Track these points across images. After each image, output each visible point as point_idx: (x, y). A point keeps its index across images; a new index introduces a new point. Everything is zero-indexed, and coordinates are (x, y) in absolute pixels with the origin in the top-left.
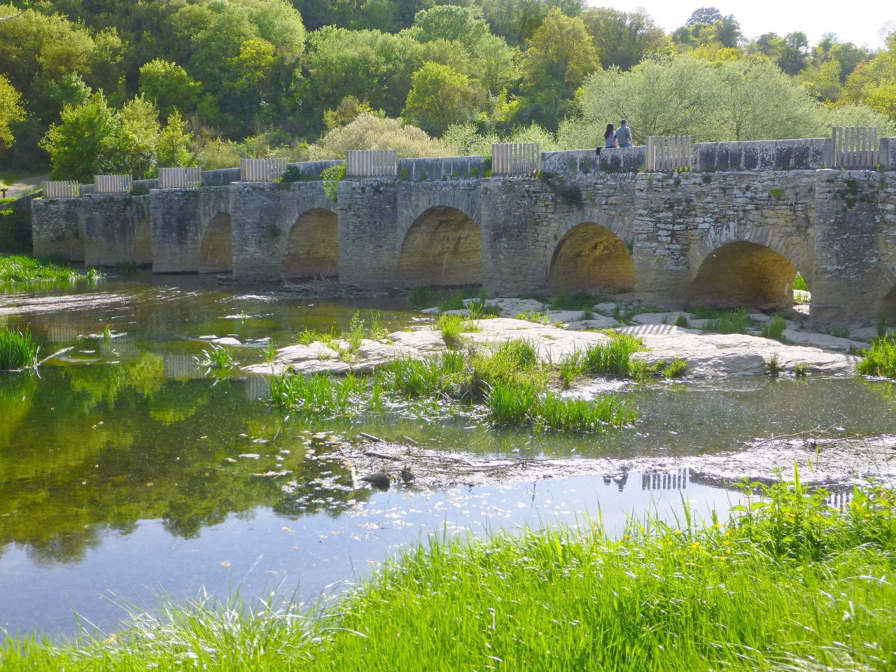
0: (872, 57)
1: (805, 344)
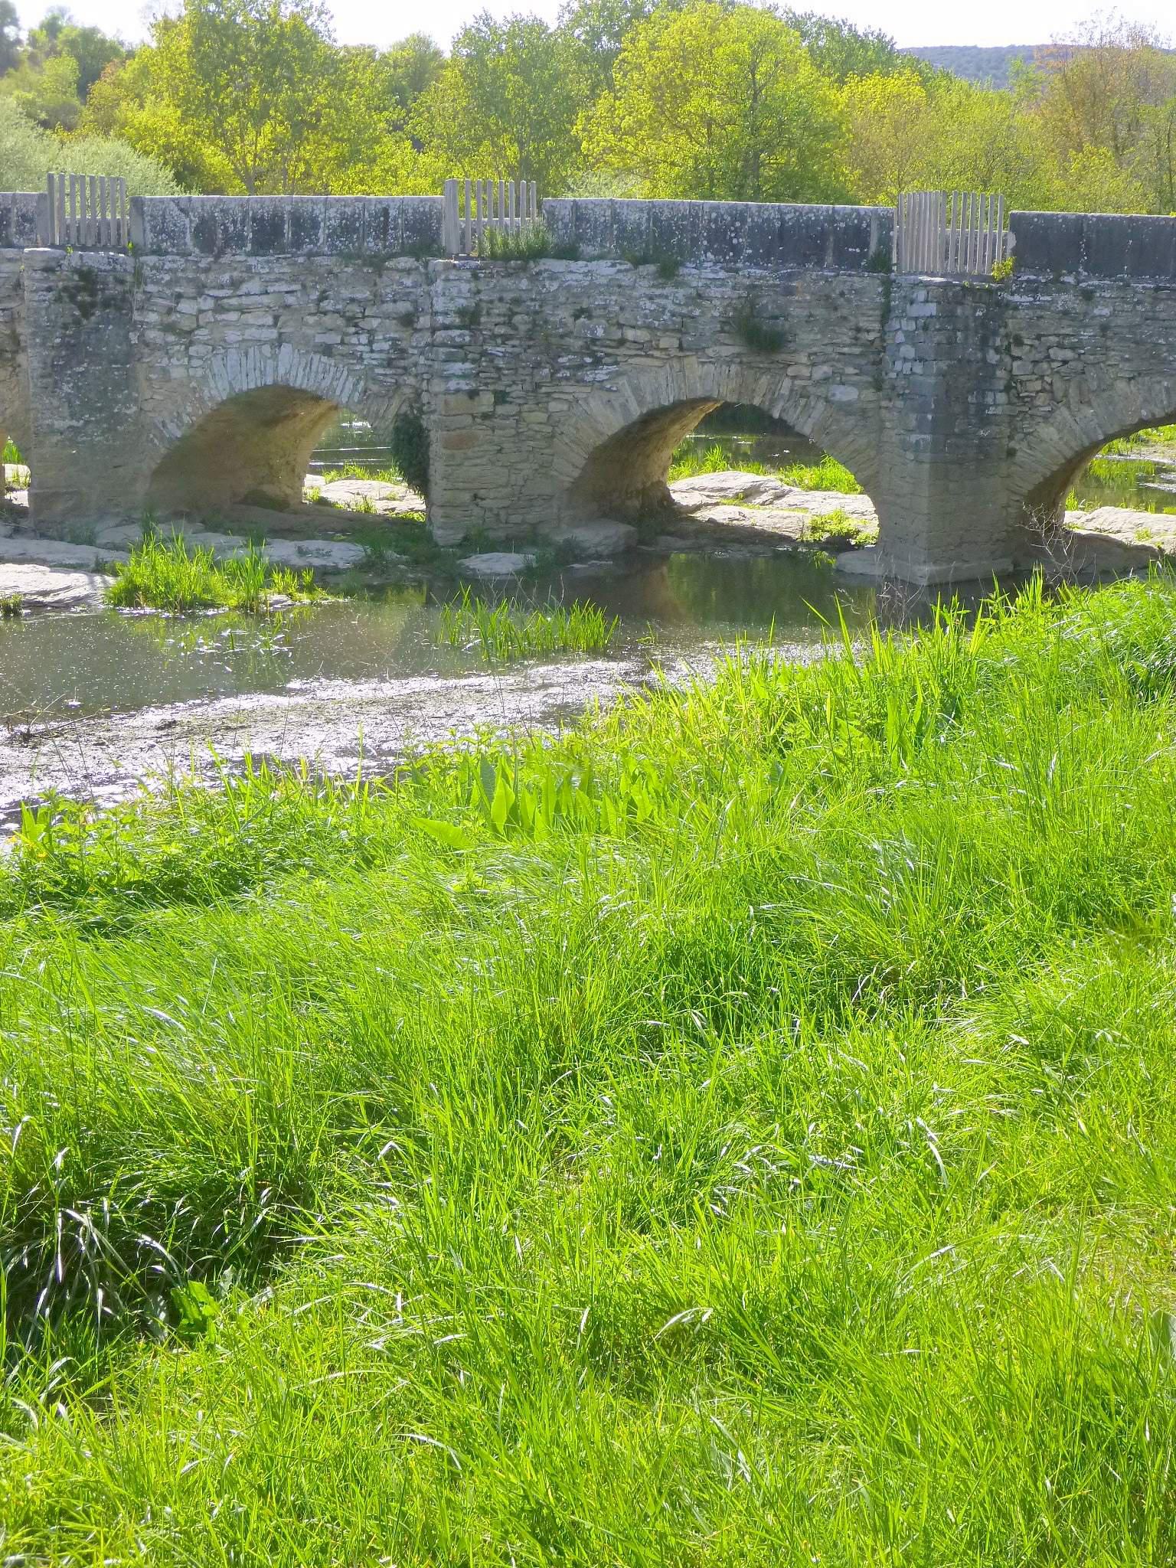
0: (131, 55)
1: (22, 559)
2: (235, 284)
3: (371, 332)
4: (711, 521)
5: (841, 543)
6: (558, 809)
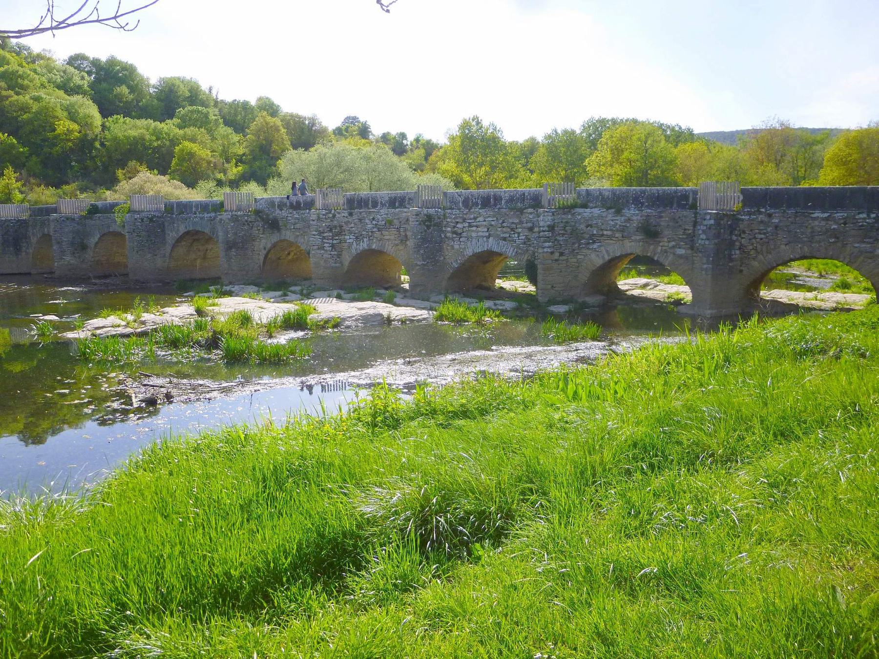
0: (441, 147)
2: (475, 218)
3: (519, 233)
4: (632, 295)
5: (678, 303)
6: (590, 392)
